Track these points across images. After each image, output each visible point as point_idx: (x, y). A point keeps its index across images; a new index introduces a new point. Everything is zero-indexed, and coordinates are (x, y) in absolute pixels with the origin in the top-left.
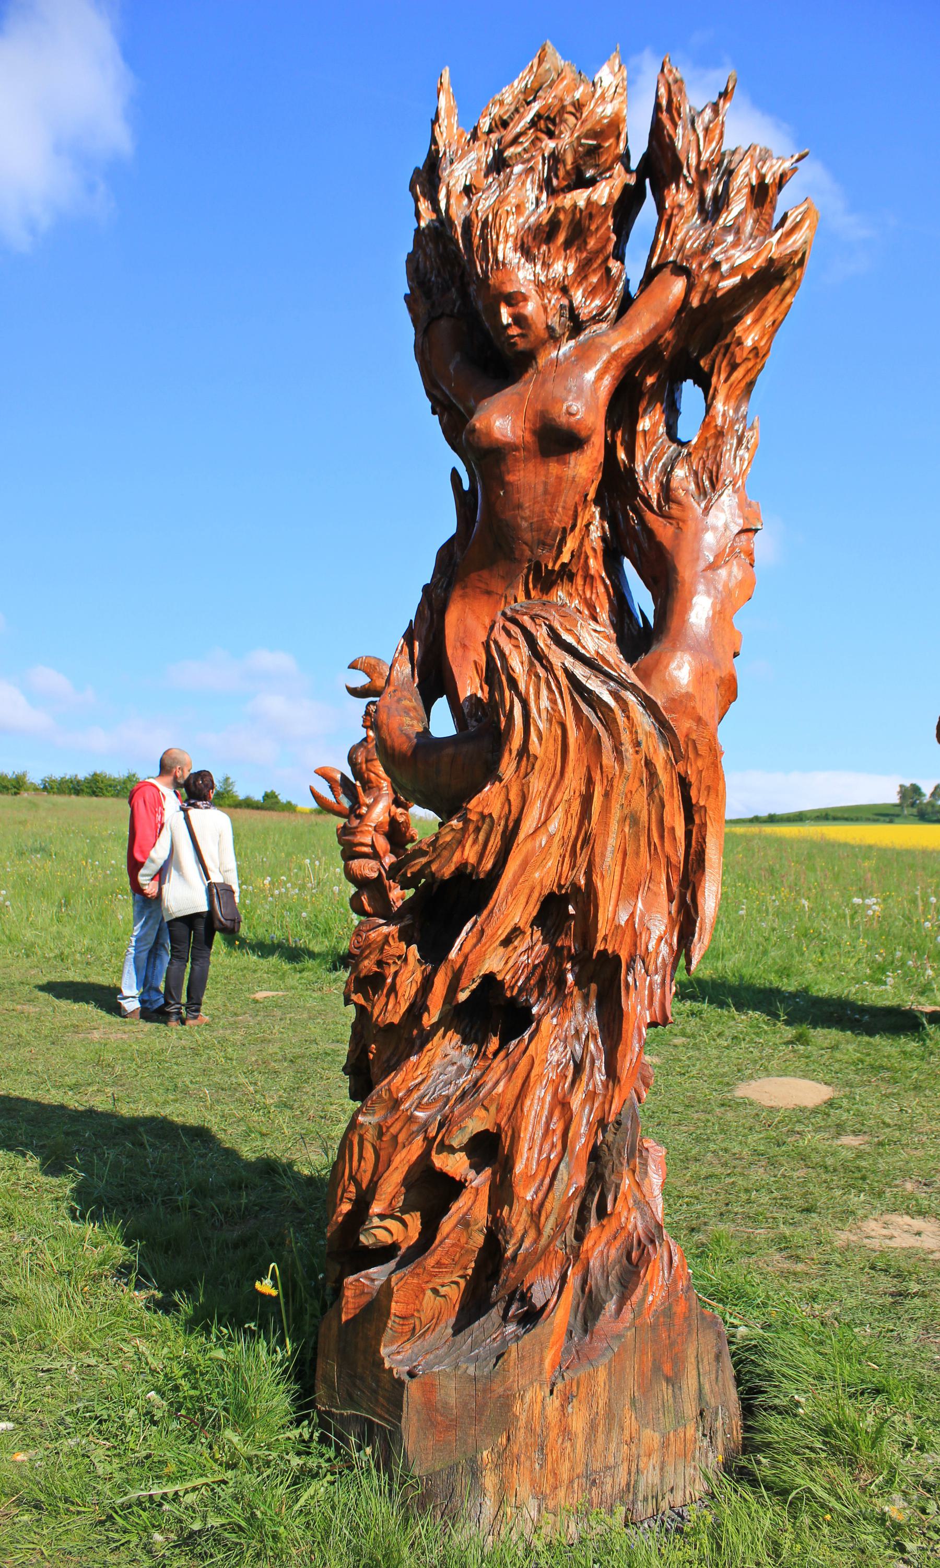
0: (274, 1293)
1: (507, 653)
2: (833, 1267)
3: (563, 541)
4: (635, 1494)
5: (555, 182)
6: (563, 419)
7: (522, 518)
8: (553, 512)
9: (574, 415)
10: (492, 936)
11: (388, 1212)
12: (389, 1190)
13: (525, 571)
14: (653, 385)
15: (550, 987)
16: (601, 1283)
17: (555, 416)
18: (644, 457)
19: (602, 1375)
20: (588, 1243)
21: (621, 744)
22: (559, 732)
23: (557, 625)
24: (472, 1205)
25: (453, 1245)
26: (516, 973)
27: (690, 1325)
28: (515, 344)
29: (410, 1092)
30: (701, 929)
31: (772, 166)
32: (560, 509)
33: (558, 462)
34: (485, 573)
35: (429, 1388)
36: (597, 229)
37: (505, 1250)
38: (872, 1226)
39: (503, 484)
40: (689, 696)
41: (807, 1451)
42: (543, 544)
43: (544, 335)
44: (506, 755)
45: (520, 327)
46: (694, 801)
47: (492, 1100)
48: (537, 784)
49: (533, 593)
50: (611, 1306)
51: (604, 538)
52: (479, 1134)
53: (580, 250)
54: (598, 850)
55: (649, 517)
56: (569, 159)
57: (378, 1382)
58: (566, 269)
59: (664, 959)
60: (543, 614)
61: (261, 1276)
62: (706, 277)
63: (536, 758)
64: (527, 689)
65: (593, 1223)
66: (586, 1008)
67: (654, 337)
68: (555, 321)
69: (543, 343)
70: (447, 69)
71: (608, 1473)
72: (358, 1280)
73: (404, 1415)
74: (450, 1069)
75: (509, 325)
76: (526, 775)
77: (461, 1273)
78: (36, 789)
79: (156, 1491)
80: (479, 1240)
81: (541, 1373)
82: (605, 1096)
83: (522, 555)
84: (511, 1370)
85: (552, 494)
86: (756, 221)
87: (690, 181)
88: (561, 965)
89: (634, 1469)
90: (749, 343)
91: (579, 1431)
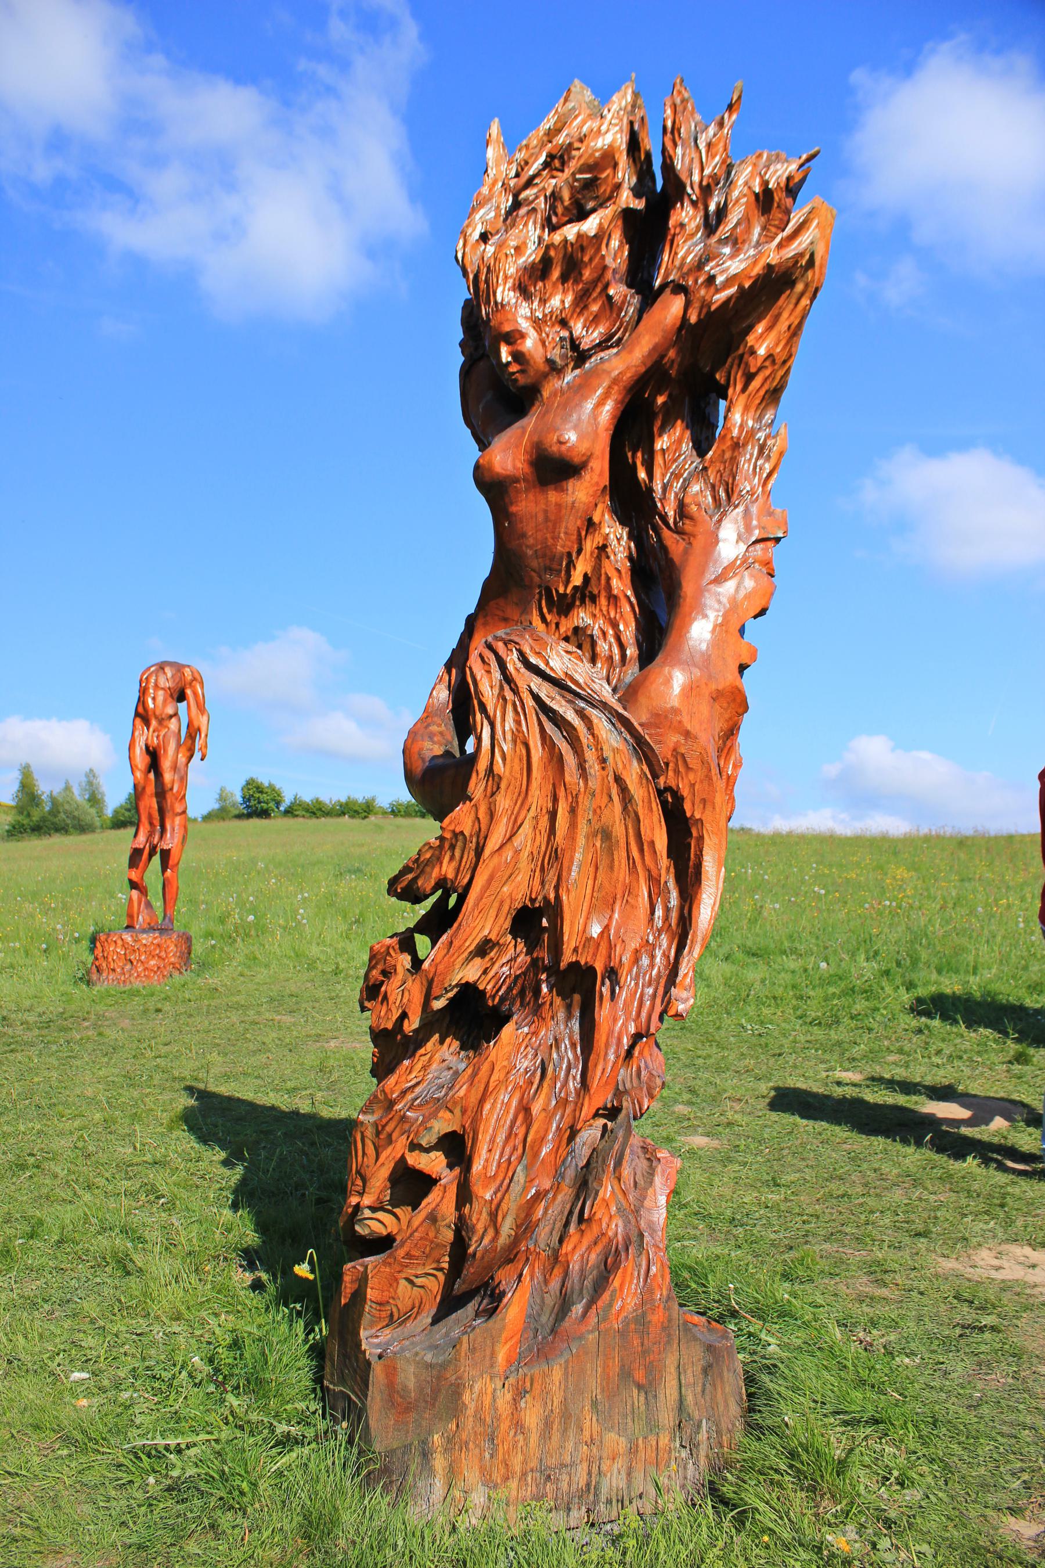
0: (311, 1277)
1: (478, 678)
2: (914, 1294)
3: (571, 564)
4: (596, 1495)
5: (554, 220)
6: (555, 448)
7: (528, 546)
8: (556, 538)
9: (564, 443)
10: (459, 948)
11: (377, 1205)
12: (378, 1184)
13: (537, 596)
14: (664, 403)
15: (529, 996)
16: (577, 1288)
17: (547, 445)
18: (664, 475)
19: (557, 1374)
20: (567, 1247)
21: (585, 761)
22: (524, 752)
23: (527, 650)
24: (441, 1200)
25: (421, 1238)
26: (497, 983)
27: (669, 1335)
28: (516, 380)
29: (404, 1093)
30: (692, 942)
31: (776, 171)
32: (562, 535)
33: (556, 489)
34: (501, 601)
35: (391, 1372)
36: (591, 260)
37: (469, 1246)
38: (985, 1256)
40: (676, 711)
41: (772, 1472)
42: (549, 569)
43: (543, 367)
44: (474, 775)
45: (520, 364)
46: (688, 814)
47: (455, 1103)
48: (504, 802)
49: (549, 617)
50: (578, 1309)
51: (630, 558)
52: (446, 1135)
53: (576, 282)
54: (566, 864)
55: (666, 533)
56: (566, 195)
57: (357, 1361)
58: (563, 302)
59: (659, 972)
60: (516, 639)
61: (300, 1260)
62: (703, 292)
63: (500, 778)
64: (495, 712)
65: (572, 1228)
66: (569, 1017)
67: (655, 357)
68: (555, 354)
69: (545, 376)
70: (496, 120)
71: (564, 1470)
72: (354, 1267)
73: (370, 1393)
74: (446, 1073)
75: (508, 364)
76: (493, 794)
77: (434, 1265)
78: (384, 813)
79: (160, 1441)
80: (449, 1235)
81: (492, 1366)
82: (576, 1104)
83: (532, 580)
84: (462, 1360)
85: (552, 520)
86: (764, 228)
87: (694, 198)
88: (536, 974)
89: (595, 1470)
90: (762, 351)
91: (533, 1426)
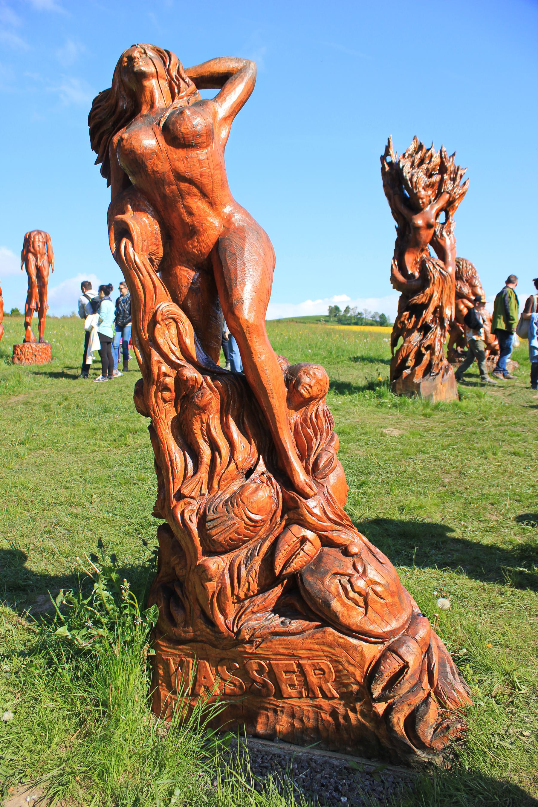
39: (419, 234)
